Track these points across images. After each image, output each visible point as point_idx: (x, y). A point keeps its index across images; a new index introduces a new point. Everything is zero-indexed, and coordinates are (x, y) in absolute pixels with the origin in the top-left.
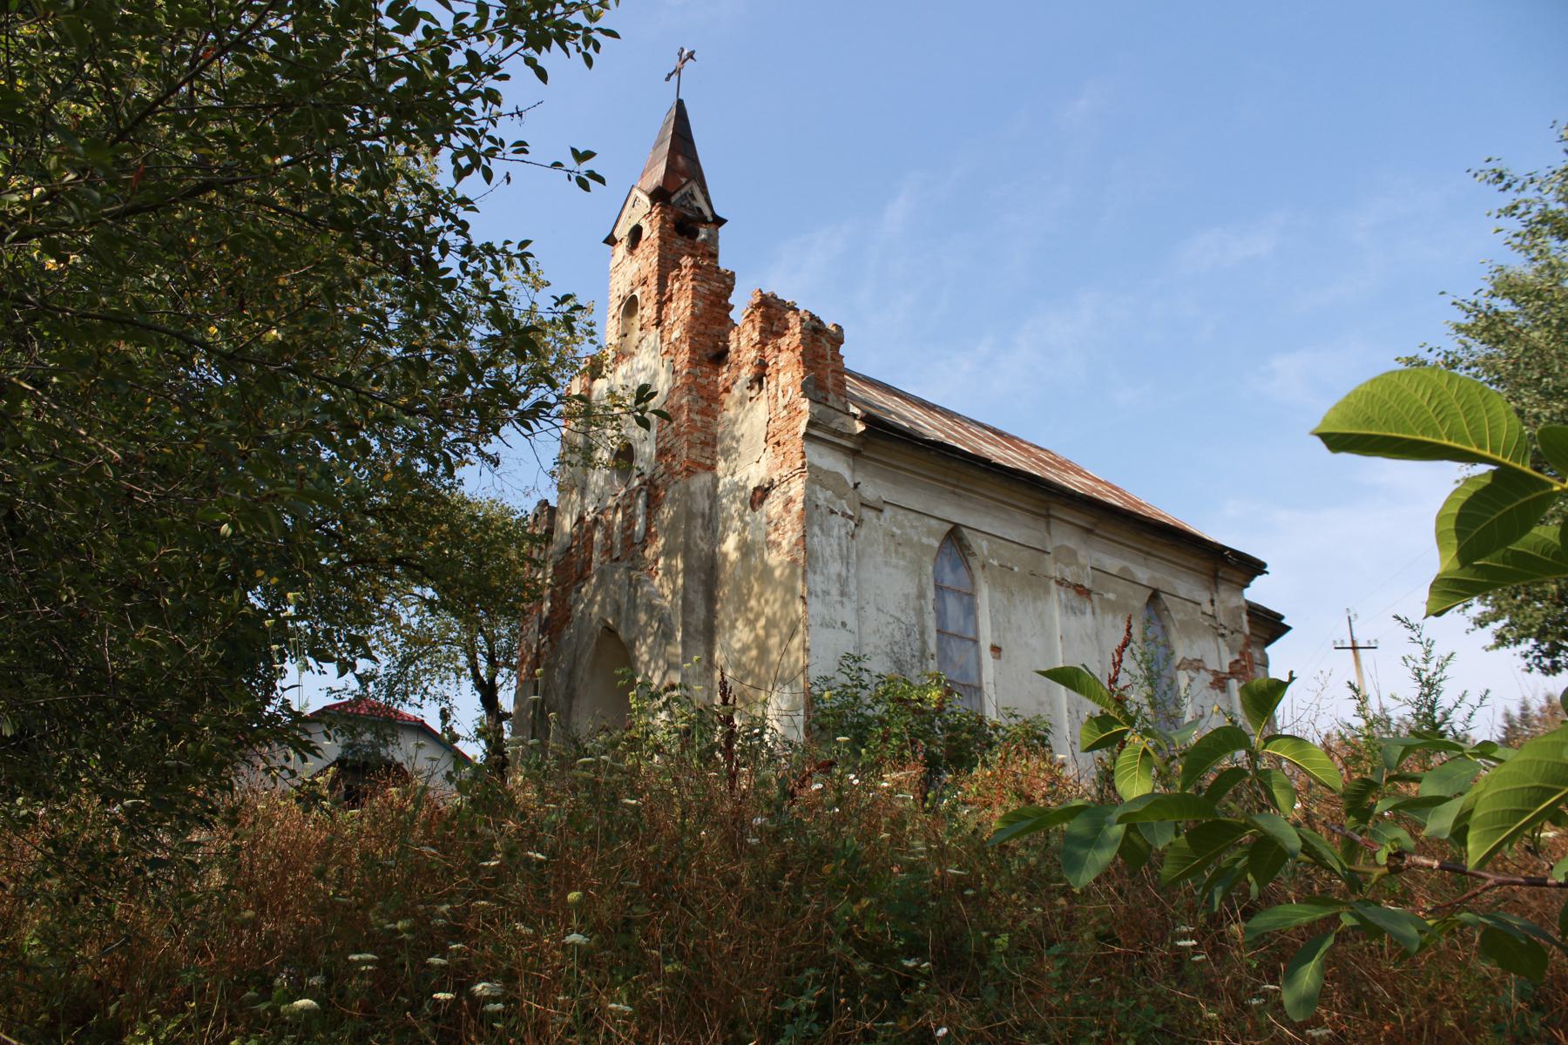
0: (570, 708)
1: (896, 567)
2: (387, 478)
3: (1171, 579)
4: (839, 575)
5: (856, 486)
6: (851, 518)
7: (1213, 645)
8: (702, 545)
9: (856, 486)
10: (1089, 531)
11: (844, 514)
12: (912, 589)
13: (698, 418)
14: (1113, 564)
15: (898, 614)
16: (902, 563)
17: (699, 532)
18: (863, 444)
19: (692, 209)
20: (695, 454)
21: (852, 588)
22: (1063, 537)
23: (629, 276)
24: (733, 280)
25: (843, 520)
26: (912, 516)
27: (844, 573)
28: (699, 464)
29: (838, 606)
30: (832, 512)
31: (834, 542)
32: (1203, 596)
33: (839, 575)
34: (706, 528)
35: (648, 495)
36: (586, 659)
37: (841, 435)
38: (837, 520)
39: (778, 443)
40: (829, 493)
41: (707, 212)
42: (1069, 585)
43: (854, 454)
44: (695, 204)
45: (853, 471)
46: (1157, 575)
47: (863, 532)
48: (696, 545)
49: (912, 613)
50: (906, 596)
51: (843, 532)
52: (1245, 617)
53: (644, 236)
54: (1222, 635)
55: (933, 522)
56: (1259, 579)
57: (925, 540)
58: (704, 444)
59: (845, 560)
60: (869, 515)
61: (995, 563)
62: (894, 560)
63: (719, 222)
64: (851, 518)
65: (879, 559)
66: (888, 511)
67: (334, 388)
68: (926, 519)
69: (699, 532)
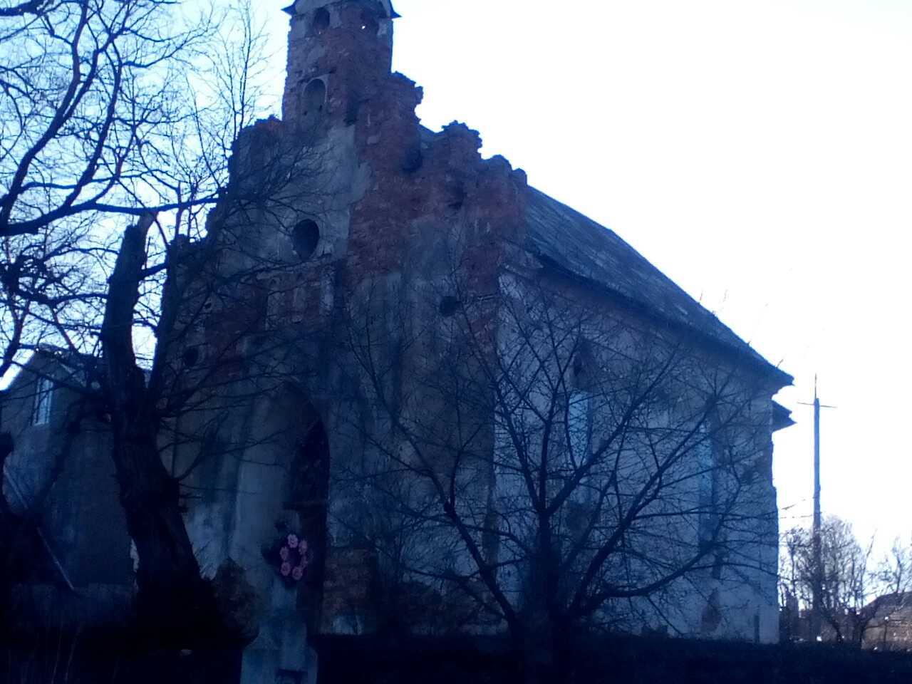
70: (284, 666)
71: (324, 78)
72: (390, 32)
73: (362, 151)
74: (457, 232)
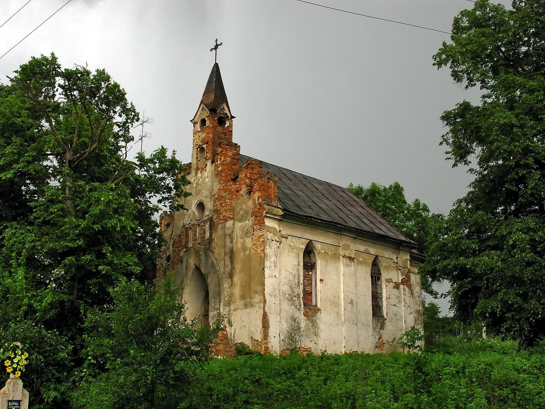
1: (291, 256)
5: (280, 231)
6: (278, 242)
7: (396, 273)
9: (280, 231)
10: (355, 238)
12: (296, 263)
13: (228, 201)
14: (362, 248)
21: (278, 265)
28: (229, 217)
32: (394, 257)
35: (210, 224)
37: (276, 215)
38: (274, 242)
41: (229, 115)
42: (347, 257)
44: (225, 112)
45: (279, 226)
46: (378, 250)
47: (281, 246)
50: (294, 265)
52: (409, 262)
54: (400, 269)
59: (276, 256)
60: (283, 240)
64: (278, 242)
66: (289, 237)
70: (11, 399)
71: (204, 146)
72: (231, 125)
73: (217, 174)
74: (250, 203)
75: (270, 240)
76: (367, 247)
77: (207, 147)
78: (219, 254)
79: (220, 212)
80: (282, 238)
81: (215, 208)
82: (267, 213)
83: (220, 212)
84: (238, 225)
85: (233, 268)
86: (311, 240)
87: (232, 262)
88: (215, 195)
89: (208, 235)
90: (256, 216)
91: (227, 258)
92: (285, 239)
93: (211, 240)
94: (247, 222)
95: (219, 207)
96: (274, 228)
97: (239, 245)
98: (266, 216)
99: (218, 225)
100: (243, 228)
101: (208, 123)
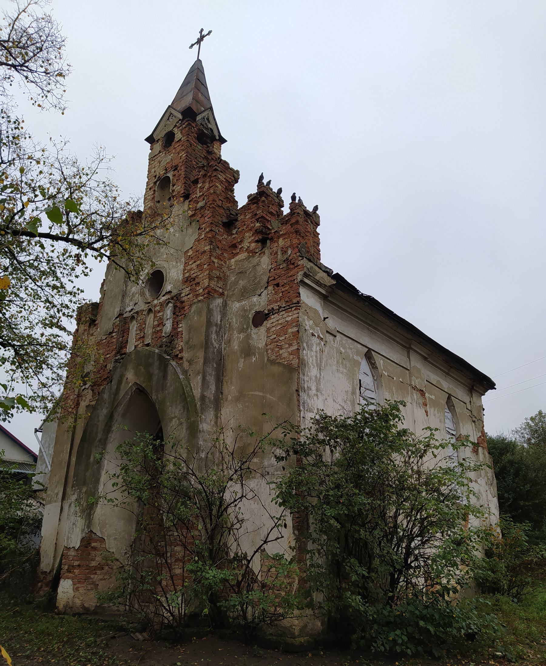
0: (106, 439)
1: (342, 373)
2: (308, 556)
3: (455, 389)
4: (316, 377)
8: (216, 345)
9: (325, 319)
10: (425, 359)
11: (319, 336)
12: (350, 390)
13: (216, 261)
14: (434, 377)
15: (343, 404)
16: (345, 371)
17: (214, 336)
18: (330, 293)
19: (207, 129)
20: (213, 284)
22: (416, 363)
23: (163, 164)
24: (239, 175)
25: (318, 341)
26: (351, 341)
27: (318, 376)
28: (215, 290)
29: (315, 398)
30: (313, 335)
31: (313, 354)
33: (316, 377)
34: (217, 333)
35: (175, 307)
36: (120, 409)
39: (278, 285)
40: (311, 322)
43: (324, 298)
44: (210, 126)
48: (212, 344)
49: (349, 403)
50: (347, 392)
51: (318, 348)
53: (176, 139)
54: (474, 422)
55: (359, 346)
56: (490, 391)
57: (355, 357)
58: (219, 278)
60: (330, 338)
61: (386, 374)
62: (341, 369)
63: (223, 141)
65: (334, 368)
67: (245, 606)
68: (356, 344)
69: (214, 336)
75: (310, 335)
76: (439, 379)
77: (174, 175)
78: (190, 362)
79: (197, 280)
80: (328, 335)
81: (187, 275)
82: (306, 275)
83: (197, 280)
84: (235, 306)
85: (219, 391)
86: (370, 349)
87: (219, 381)
88: (187, 251)
89: (168, 327)
90: (278, 285)
91: (210, 370)
92: (331, 338)
93: (174, 334)
94: (255, 299)
95: (195, 272)
96: (316, 311)
97: (236, 346)
98: (302, 281)
99: (191, 305)
100: (246, 311)
101: (178, 135)
